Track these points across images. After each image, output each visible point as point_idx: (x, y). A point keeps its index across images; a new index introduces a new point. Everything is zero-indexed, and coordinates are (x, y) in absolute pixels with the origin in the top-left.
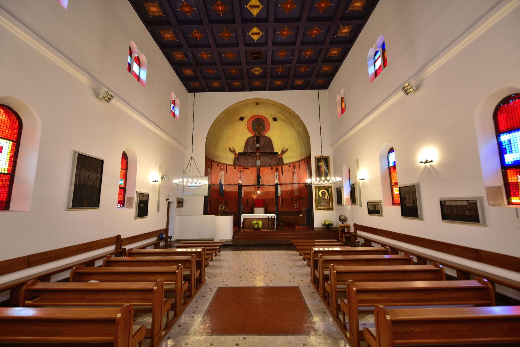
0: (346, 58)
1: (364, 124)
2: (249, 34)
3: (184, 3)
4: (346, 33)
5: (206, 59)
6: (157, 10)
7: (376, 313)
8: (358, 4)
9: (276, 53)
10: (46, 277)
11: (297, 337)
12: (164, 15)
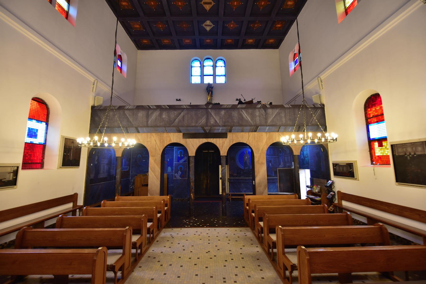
0: (301, 11)
1: (376, 37)
2: (203, 25)
3: (154, 8)
4: (291, 5)
5: (161, 29)
6: (127, 5)
7: (298, 253)
8: (290, 3)
9: (226, 25)
10: (40, 224)
11: (236, 269)
12: (133, 9)
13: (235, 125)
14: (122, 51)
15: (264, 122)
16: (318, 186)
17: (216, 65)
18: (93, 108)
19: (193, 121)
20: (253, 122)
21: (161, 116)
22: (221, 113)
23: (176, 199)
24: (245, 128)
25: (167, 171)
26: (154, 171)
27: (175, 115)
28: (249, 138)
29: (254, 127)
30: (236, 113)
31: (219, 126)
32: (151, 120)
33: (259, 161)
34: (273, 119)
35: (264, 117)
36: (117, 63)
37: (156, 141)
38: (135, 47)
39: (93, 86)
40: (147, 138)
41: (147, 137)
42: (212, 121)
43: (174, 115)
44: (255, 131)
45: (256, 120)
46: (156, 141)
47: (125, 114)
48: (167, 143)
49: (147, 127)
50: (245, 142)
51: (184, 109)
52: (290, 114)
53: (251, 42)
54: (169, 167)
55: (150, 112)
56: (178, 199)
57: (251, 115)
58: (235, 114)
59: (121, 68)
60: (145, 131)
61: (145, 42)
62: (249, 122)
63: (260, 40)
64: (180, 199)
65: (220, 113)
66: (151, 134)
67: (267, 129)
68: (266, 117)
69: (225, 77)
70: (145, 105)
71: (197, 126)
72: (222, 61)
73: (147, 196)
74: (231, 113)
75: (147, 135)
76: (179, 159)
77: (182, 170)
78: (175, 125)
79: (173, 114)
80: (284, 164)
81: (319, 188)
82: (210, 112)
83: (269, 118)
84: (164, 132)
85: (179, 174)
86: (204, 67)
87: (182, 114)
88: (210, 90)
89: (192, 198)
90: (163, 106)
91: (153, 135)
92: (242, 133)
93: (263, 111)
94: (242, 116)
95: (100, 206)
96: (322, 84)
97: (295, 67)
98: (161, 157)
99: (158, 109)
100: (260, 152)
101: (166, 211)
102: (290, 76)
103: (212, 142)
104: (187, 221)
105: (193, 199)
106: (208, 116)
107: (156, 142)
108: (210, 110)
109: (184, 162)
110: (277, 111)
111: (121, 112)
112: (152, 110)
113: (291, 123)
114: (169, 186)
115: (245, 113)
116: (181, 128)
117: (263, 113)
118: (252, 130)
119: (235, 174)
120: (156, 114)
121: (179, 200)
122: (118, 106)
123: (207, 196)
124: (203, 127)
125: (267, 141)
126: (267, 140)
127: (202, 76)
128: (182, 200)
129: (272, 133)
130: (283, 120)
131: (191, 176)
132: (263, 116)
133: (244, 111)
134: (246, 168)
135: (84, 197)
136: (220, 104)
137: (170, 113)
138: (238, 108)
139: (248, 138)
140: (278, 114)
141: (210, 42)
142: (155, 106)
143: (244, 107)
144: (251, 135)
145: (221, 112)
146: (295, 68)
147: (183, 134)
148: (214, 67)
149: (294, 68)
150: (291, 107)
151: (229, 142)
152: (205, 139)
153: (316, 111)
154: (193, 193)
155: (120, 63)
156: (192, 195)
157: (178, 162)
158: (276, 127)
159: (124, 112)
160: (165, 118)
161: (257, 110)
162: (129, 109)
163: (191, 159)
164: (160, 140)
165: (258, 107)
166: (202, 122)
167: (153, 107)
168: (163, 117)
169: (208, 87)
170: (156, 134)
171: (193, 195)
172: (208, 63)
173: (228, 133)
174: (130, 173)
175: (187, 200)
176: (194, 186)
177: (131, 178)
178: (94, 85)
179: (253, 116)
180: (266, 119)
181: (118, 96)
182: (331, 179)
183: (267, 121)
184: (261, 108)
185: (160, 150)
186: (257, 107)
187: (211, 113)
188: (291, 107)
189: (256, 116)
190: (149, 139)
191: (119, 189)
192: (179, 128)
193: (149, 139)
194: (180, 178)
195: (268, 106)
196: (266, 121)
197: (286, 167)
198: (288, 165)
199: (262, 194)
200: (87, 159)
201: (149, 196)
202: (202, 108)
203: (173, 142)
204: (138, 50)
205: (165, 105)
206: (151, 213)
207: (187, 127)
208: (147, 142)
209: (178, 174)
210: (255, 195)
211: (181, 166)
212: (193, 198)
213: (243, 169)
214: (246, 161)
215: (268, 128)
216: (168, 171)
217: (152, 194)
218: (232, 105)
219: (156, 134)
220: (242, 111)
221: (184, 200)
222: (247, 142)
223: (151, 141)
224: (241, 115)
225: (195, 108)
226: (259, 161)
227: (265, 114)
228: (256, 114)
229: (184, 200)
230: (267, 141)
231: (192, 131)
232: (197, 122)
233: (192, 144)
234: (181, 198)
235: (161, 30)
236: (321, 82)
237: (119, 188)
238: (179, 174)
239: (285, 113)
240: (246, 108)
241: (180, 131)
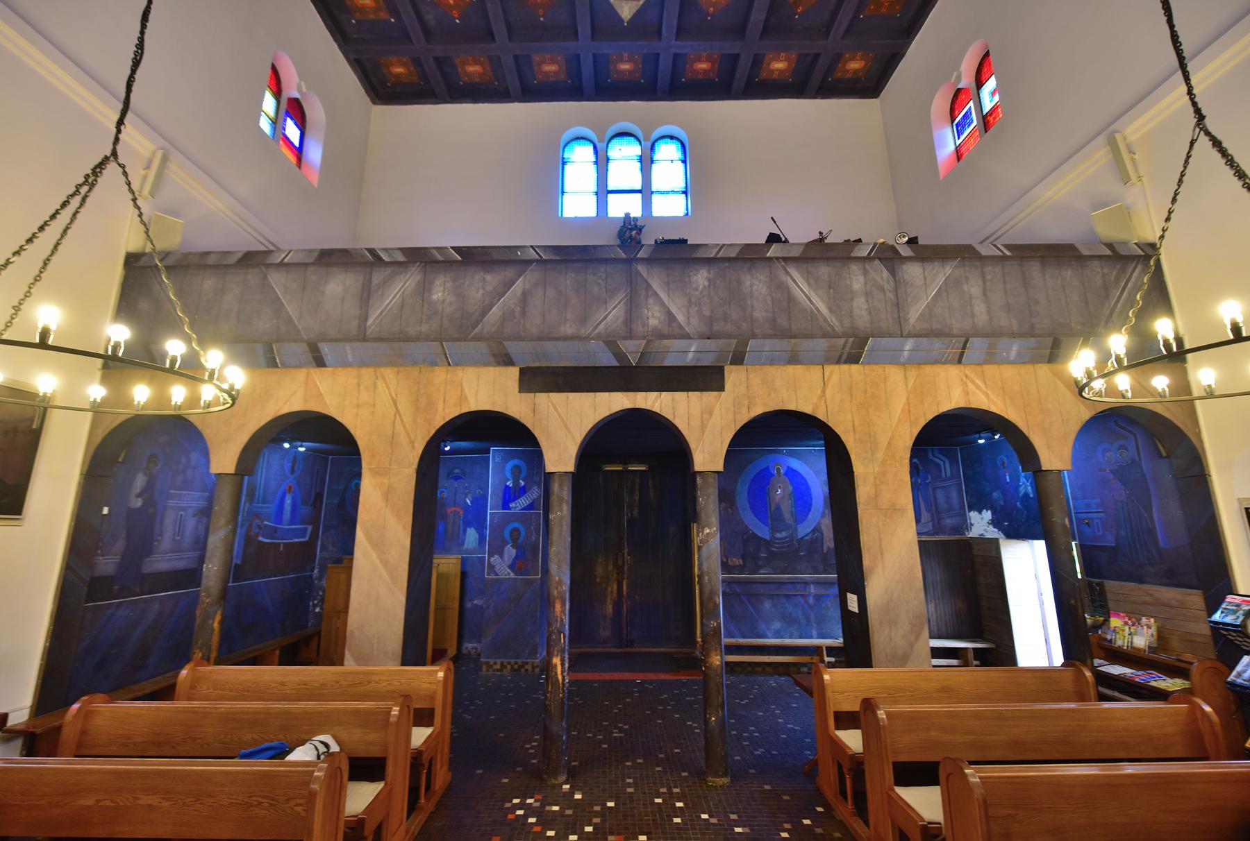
13: (757, 331)
14: (303, 84)
15: (891, 320)
16: (1144, 620)
17: (652, 158)
18: (133, 261)
19: (569, 316)
20: (841, 321)
21: (426, 295)
22: (694, 279)
23: (492, 661)
24: (805, 345)
25: (463, 543)
26: (378, 544)
27: (489, 288)
28: (824, 392)
29: (846, 342)
30: (760, 281)
31: (687, 336)
32: (382, 312)
33: (876, 496)
34: (930, 307)
35: (891, 296)
36: (284, 129)
37: (395, 403)
38: (363, 90)
39: (143, 172)
40: (359, 391)
41: (359, 385)
42: (653, 316)
43: (481, 292)
44: (854, 359)
45: (851, 314)
46: (395, 403)
47: (265, 285)
48: (447, 411)
49: (358, 340)
50: (807, 409)
51: (528, 262)
52: (1005, 283)
53: (781, 71)
54: (468, 529)
55: (378, 276)
56: (499, 661)
57: (830, 287)
58: (756, 284)
59: (299, 152)
60: (350, 356)
61: (398, 75)
62: (821, 319)
63: (817, 56)
64: (509, 663)
65: (687, 280)
66: (375, 373)
67: (907, 348)
68: (897, 297)
69: (687, 196)
70: (355, 249)
71: (587, 338)
72: (674, 141)
73: (342, 664)
74: (739, 282)
75: (359, 377)
76: (509, 496)
77: (519, 542)
78: (485, 330)
79: (479, 284)
80: (933, 520)
81: (1149, 627)
82: (645, 275)
83: (909, 299)
84: (434, 364)
85: (506, 555)
86: (608, 162)
87: (519, 285)
88: (631, 236)
89: (560, 677)
90: (435, 252)
91: (384, 379)
92: (791, 369)
93: (880, 273)
94: (789, 292)
95: (166, 693)
96: (1133, 160)
97: (958, 142)
98: (415, 475)
99: (415, 262)
100: (880, 455)
101: (417, 756)
102: (941, 178)
103: (656, 409)
104: (530, 811)
105: (563, 684)
106: (636, 294)
107: (397, 408)
108: (641, 268)
109: (531, 506)
110: (942, 273)
111: (253, 276)
112: (389, 270)
113: (1015, 324)
114: (469, 605)
115: (801, 280)
116: (512, 347)
117: (882, 278)
118: (838, 355)
119: (737, 561)
120: (407, 282)
121: (506, 667)
122: (240, 252)
123: (620, 650)
124: (611, 344)
125: (909, 404)
126: (908, 399)
127: (603, 192)
128: (516, 667)
129: (929, 370)
130: (977, 309)
131: (553, 567)
132: (884, 291)
133: (796, 273)
134: (778, 535)
135: (41, 665)
136: (689, 243)
137: (467, 283)
138: (770, 259)
139: (819, 392)
140: (952, 285)
141: (630, 71)
142: (401, 249)
143: (797, 255)
144: (835, 377)
145: (696, 275)
146: (957, 148)
147: (523, 372)
148: (646, 162)
149: (952, 148)
150: (1008, 253)
151: (732, 409)
152: (619, 394)
153: (1123, 270)
154: (563, 651)
155: (299, 132)
156: (556, 665)
157: (505, 505)
158: (947, 340)
159: (265, 277)
160: (443, 301)
161: (855, 268)
162: (288, 265)
163: (555, 487)
164: (417, 400)
165: (859, 255)
166: (609, 318)
167: (393, 257)
168: (435, 297)
169: (624, 226)
170: (398, 372)
171: (563, 665)
172: (624, 154)
173: (728, 368)
174: (318, 553)
175: (537, 666)
176: (566, 620)
177: (319, 572)
178: (148, 167)
179: (838, 295)
180: (899, 306)
181: (274, 242)
182: (1237, 590)
183: (901, 315)
184: (873, 259)
185: (412, 442)
186: (852, 255)
187: (650, 281)
188: (1008, 253)
189: (852, 292)
190: (365, 396)
191: (213, 630)
192: (504, 346)
193: (365, 396)
194: (512, 576)
195: (905, 251)
196: (899, 317)
197: (944, 533)
198: (949, 522)
199: (902, 659)
200: (79, 483)
201: (350, 664)
202: (607, 261)
203: (474, 408)
204: (374, 103)
205: (446, 248)
206: (299, 809)
207: (540, 339)
208: (358, 406)
209: (501, 556)
210: (871, 666)
211: (516, 525)
212: (563, 677)
213: (767, 537)
214: (778, 508)
215: (909, 344)
216: (465, 546)
217: (361, 659)
218: (742, 244)
219: (398, 372)
220: (787, 273)
221: (526, 667)
222: (816, 407)
223: (374, 405)
224: (782, 287)
225: (577, 261)
226: (876, 496)
227: (892, 283)
228: (851, 286)
229: (526, 670)
230: (909, 404)
231: (564, 356)
232: (583, 320)
233: (560, 416)
234: (513, 661)
235: (455, 19)
236: (1131, 152)
237: (211, 622)
238: (506, 559)
239: (984, 280)
240: (807, 259)
241: (507, 361)
